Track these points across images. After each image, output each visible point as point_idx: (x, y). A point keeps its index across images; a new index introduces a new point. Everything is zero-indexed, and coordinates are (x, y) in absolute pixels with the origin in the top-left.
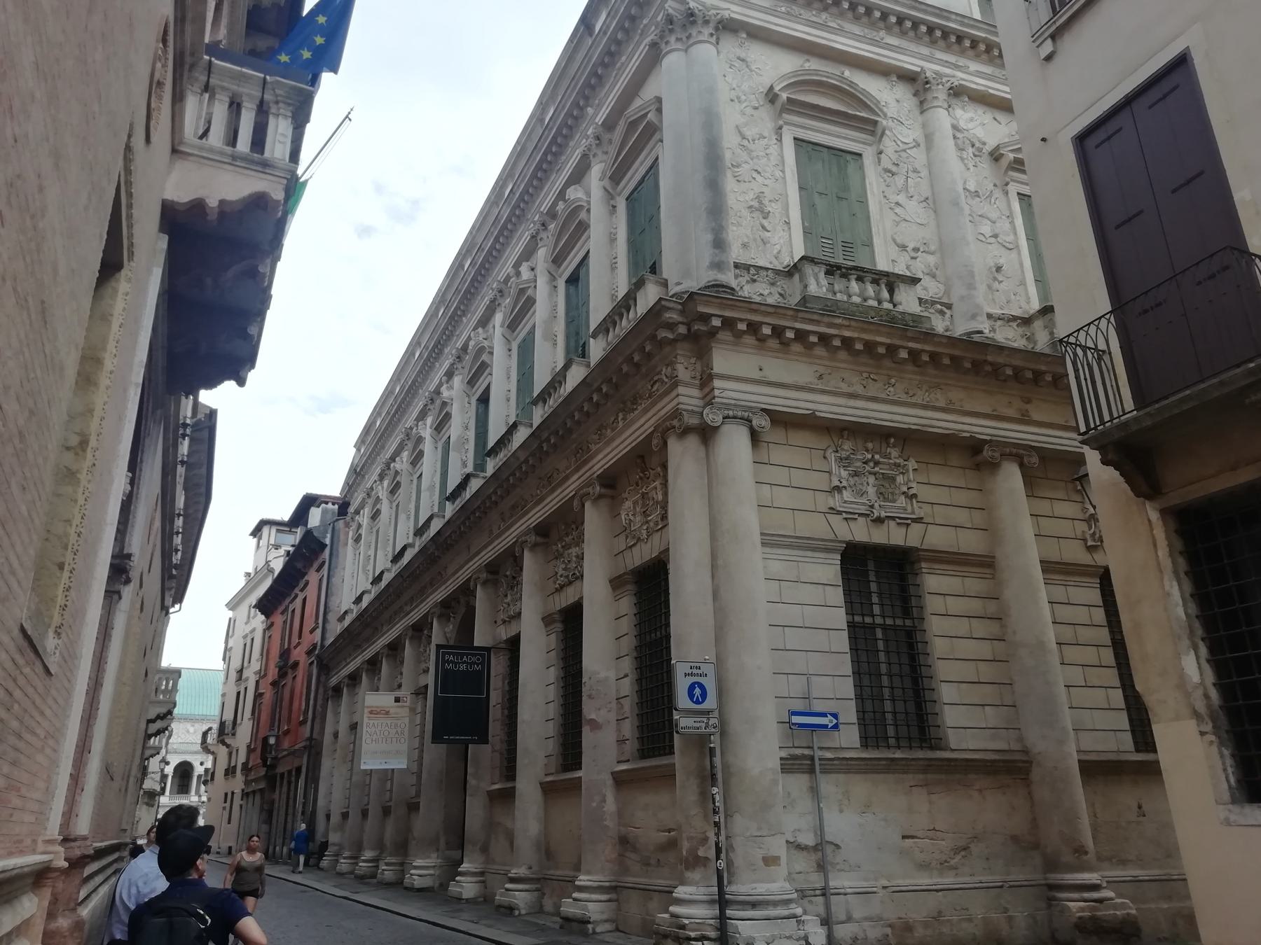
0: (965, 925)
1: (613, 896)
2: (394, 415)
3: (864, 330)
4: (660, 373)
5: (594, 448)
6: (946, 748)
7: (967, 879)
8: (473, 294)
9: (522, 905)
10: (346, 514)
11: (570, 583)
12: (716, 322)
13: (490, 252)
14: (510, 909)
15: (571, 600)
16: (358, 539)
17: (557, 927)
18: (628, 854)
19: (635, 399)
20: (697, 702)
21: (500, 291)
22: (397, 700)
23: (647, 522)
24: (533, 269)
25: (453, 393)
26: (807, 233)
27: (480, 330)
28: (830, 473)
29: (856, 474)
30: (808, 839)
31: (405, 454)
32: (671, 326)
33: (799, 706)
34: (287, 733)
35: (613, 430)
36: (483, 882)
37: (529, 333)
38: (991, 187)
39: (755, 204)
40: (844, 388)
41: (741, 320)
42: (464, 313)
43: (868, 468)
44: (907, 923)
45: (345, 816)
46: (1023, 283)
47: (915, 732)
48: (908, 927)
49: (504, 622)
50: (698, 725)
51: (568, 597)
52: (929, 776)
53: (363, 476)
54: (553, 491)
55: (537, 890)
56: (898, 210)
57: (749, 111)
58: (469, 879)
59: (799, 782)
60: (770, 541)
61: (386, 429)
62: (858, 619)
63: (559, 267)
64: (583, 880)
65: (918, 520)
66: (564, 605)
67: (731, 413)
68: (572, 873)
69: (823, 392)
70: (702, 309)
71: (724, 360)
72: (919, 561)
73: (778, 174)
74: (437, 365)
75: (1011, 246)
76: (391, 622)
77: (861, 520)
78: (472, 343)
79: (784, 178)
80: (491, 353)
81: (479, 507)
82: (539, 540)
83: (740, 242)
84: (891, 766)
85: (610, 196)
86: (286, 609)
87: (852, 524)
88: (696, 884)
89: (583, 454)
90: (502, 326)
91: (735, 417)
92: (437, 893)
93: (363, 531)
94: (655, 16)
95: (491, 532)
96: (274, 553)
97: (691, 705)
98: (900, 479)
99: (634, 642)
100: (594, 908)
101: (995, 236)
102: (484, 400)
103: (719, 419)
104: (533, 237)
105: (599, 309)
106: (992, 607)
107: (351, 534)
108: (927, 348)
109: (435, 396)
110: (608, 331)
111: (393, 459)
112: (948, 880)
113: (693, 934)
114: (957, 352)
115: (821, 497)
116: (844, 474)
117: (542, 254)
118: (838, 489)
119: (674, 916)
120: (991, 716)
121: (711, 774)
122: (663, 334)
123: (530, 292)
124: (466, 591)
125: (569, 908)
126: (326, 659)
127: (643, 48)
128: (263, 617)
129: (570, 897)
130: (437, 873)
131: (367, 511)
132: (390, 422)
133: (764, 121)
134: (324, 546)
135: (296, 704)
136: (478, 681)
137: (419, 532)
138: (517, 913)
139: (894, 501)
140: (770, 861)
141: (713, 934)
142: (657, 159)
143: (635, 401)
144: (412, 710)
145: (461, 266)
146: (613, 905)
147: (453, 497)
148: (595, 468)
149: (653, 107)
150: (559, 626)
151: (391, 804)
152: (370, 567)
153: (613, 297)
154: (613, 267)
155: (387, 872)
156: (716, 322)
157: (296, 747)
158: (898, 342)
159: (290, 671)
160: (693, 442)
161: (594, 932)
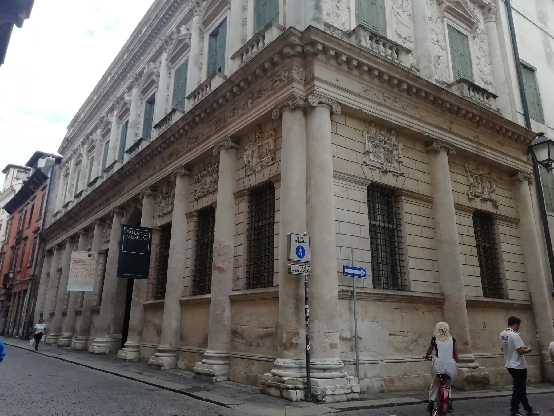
0: (416, 379)
1: (227, 361)
2: (94, 110)
3: (389, 69)
5: (229, 120)
6: (410, 290)
7: (416, 356)
8: (153, 37)
9: (166, 364)
11: (205, 195)
12: (320, 47)
13: (162, 20)
14: (159, 367)
15: (205, 205)
16: (66, 176)
17: (191, 377)
18: (236, 339)
19: (260, 91)
20: (300, 257)
22: (90, 256)
23: (261, 162)
24: (188, 30)
25: (132, 98)
26: (357, 17)
27: (152, 63)
28: (364, 144)
29: (376, 146)
30: (347, 335)
32: (293, 46)
33: (346, 263)
34: (19, 272)
35: (243, 110)
36: (139, 351)
37: (183, 64)
38: (437, 17)
40: (375, 99)
41: (333, 49)
42: (142, 54)
43: (382, 144)
44: (391, 379)
45: (52, 315)
46: (448, 67)
47: (390, 282)
48: (392, 381)
50: (300, 269)
51: (205, 203)
52: (402, 304)
53: (72, 143)
55: (175, 356)
56: (398, 16)
58: (131, 349)
59: (345, 303)
60: (338, 175)
61: (88, 117)
62: (373, 222)
63: (144, 95)
64: (209, 352)
65: (402, 175)
66: (162, 224)
67: (323, 100)
68: (158, 345)
70: (314, 37)
71: (320, 70)
72: (401, 195)
74: (122, 83)
75: (444, 48)
76: (86, 216)
77: (377, 170)
78: (145, 71)
80: (158, 76)
81: (149, 154)
82: (187, 172)
84: (387, 298)
86: (22, 210)
87: (373, 172)
88: (290, 358)
89: (221, 124)
90: (166, 60)
91: (324, 103)
92: (111, 355)
93: (70, 172)
94: (132, 74)
95: (155, 168)
96: (15, 182)
97: (297, 258)
98: (395, 152)
99: (247, 227)
100: (217, 368)
101: (438, 41)
102: (151, 102)
103: (316, 103)
104: (191, 10)
105: (158, 117)
106: (430, 223)
107: (62, 173)
108: (416, 85)
109: (119, 100)
110: (242, 56)
111: (91, 134)
112: (409, 357)
113: (290, 386)
114: (428, 90)
116: (371, 145)
117: (196, 20)
118: (368, 152)
119: (274, 375)
120: (428, 276)
121: (304, 298)
122: (287, 50)
124: (137, 200)
125: (199, 367)
126: (44, 236)
127: (187, 10)
128: (8, 214)
129: (200, 361)
130: (108, 345)
131: (73, 161)
132: (91, 114)
134: (46, 178)
135: (25, 258)
136: (145, 245)
137: (77, 196)
138: (163, 368)
139: (392, 163)
140: (333, 346)
141: (301, 386)
142: (226, 18)
143: (260, 92)
144: (97, 262)
145: (106, 79)
146: (227, 366)
147: (130, 151)
149: (188, 37)
150: (195, 219)
151: (84, 311)
152: (74, 190)
153: (243, 40)
154: (244, 24)
155: (77, 343)
156: (320, 47)
157: (25, 279)
158: (404, 79)
159: (23, 241)
160: (299, 115)
161: (216, 381)
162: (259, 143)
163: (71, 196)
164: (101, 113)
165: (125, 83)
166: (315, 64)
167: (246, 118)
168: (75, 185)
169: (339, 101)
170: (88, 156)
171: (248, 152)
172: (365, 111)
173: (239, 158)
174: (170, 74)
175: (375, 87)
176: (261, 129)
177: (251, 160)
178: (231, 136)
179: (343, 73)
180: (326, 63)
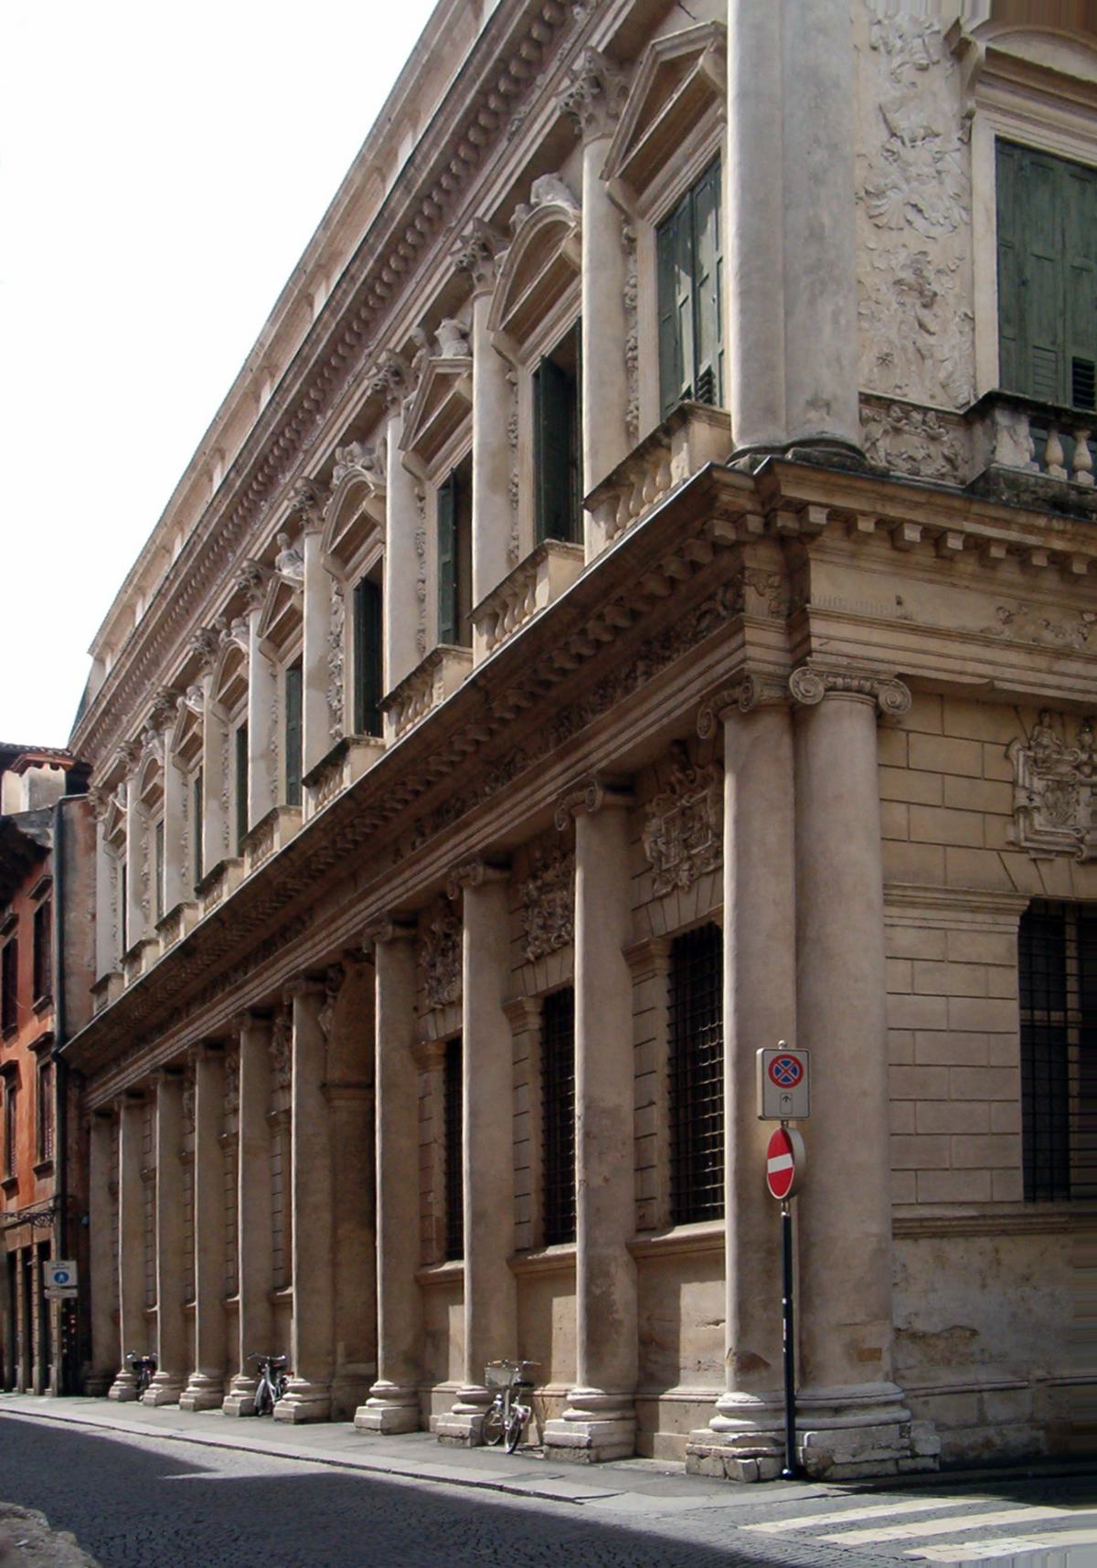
4: (711, 597)
10: (85, 788)
11: (554, 952)
16: (118, 840)
21: (397, 373)
23: (690, 858)
27: (355, 447)
28: (1014, 783)
29: (1061, 785)
31: (206, 683)
32: (737, 519)
35: (627, 691)
39: (907, 275)
42: (319, 407)
49: (433, 1010)
54: (516, 790)
57: (908, 73)
66: (442, 1034)
69: (1009, 645)
71: (828, 584)
73: (957, 214)
74: (265, 506)
78: (338, 472)
79: (970, 224)
83: (875, 353)
85: (623, 216)
87: (1044, 868)
90: (402, 447)
91: (847, 689)
93: (127, 825)
111: (181, 686)
115: (996, 825)
116: (1038, 785)
118: (1025, 811)
123: (458, 385)
132: (167, 614)
133: (940, 96)
134: (43, 852)
147: (318, 778)
148: (593, 758)
154: (629, 366)
162: (681, 797)
163: (147, 918)
164: (204, 614)
165: (273, 509)
166: (813, 565)
167: (637, 720)
168: (153, 876)
169: (901, 669)
170: (185, 774)
171: (655, 824)
172: (1007, 686)
173: (634, 840)
174: (421, 499)
175: (1050, 599)
176: (685, 752)
177: (663, 848)
178: (602, 772)
179: (920, 575)
180: (853, 556)
